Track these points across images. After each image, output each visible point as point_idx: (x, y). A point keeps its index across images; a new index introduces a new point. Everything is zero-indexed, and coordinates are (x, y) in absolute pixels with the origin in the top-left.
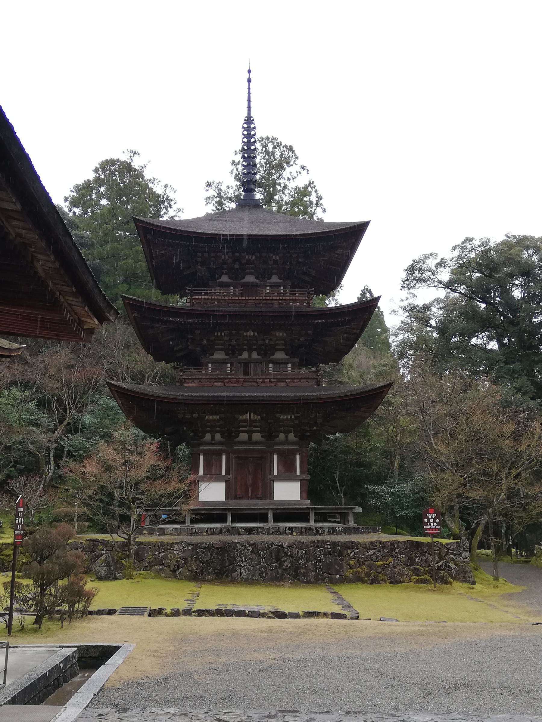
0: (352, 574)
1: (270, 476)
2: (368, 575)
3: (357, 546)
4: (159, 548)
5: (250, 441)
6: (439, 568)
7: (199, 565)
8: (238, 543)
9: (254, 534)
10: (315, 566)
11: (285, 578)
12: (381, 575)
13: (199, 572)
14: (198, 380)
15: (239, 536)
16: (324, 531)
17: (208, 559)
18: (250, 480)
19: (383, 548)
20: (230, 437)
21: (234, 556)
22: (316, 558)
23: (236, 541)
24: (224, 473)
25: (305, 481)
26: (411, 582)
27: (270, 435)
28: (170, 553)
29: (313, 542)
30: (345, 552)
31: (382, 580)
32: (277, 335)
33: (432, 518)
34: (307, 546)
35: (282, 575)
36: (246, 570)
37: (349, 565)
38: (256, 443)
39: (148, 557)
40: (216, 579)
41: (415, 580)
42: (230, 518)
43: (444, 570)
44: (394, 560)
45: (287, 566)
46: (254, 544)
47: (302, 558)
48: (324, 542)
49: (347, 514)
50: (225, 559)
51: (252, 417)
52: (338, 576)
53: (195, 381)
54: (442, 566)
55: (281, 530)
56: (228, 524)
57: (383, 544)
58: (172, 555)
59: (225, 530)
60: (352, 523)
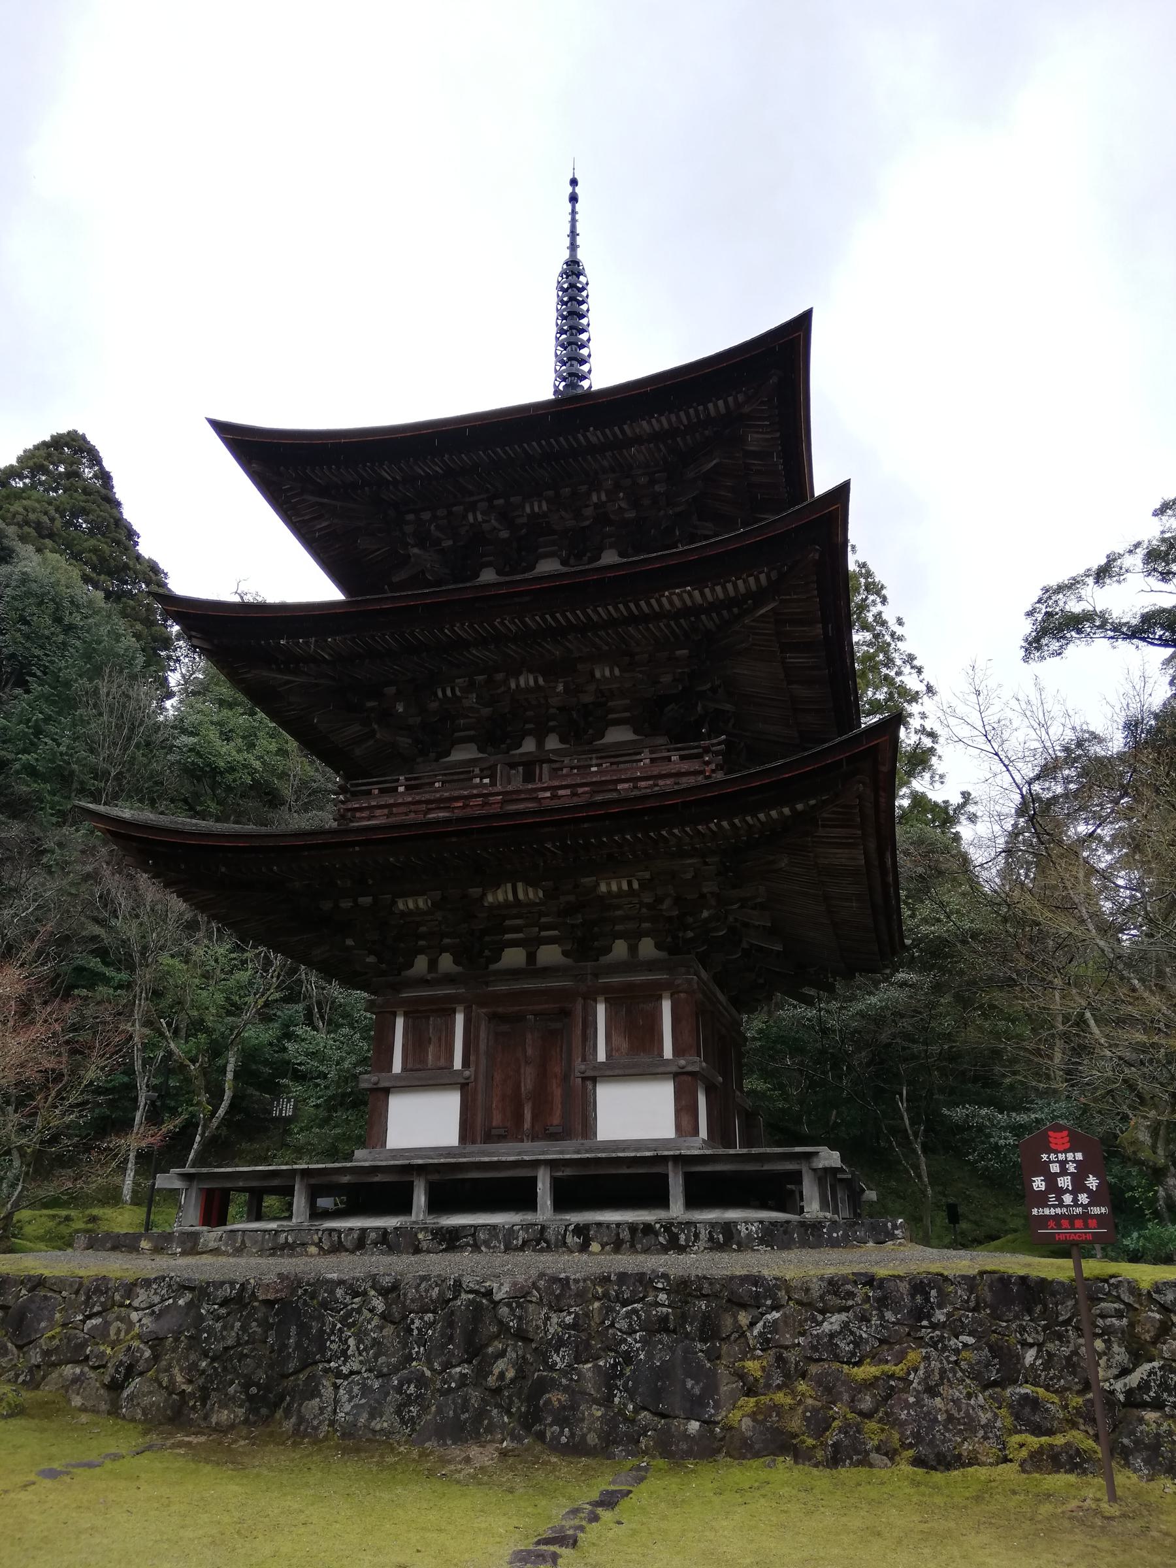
0: (753, 1415)
1: (579, 1066)
2: (819, 1424)
3: (774, 1298)
4: (89, 1298)
5: (532, 969)
6: (1134, 1400)
7: (194, 1366)
8: (341, 1282)
9: (462, 1248)
10: (609, 1378)
11: (490, 1430)
12: (872, 1425)
13: (192, 1394)
14: (386, 811)
15: (498, 1260)
16: (697, 1236)
17: (230, 1342)
18: (528, 1087)
19: (883, 1303)
20: (477, 953)
21: (321, 1331)
22: (611, 1347)
23: (334, 1276)
24: (458, 1064)
25: (685, 1078)
26: (1006, 1460)
27: (585, 946)
28: (118, 1318)
29: (605, 1280)
30: (728, 1321)
31: (878, 1449)
32: (598, 675)
33: (1064, 1172)
34: (582, 1297)
35: (481, 1414)
36: (356, 1389)
37: (741, 1375)
38: (547, 972)
39: (49, 1334)
40: (246, 1421)
41: (1024, 1453)
42: (420, 1199)
43: (1157, 1405)
44: (927, 1358)
45: (502, 1375)
46: (395, 1287)
47: (560, 1343)
48: (644, 1281)
49: (797, 1177)
50: (286, 1346)
51: (521, 896)
52: (694, 1426)
53: (378, 812)
54: (1144, 1386)
55: (550, 1234)
56: (413, 1218)
57: (881, 1286)
58: (123, 1326)
59: (373, 1235)
60: (813, 1208)
